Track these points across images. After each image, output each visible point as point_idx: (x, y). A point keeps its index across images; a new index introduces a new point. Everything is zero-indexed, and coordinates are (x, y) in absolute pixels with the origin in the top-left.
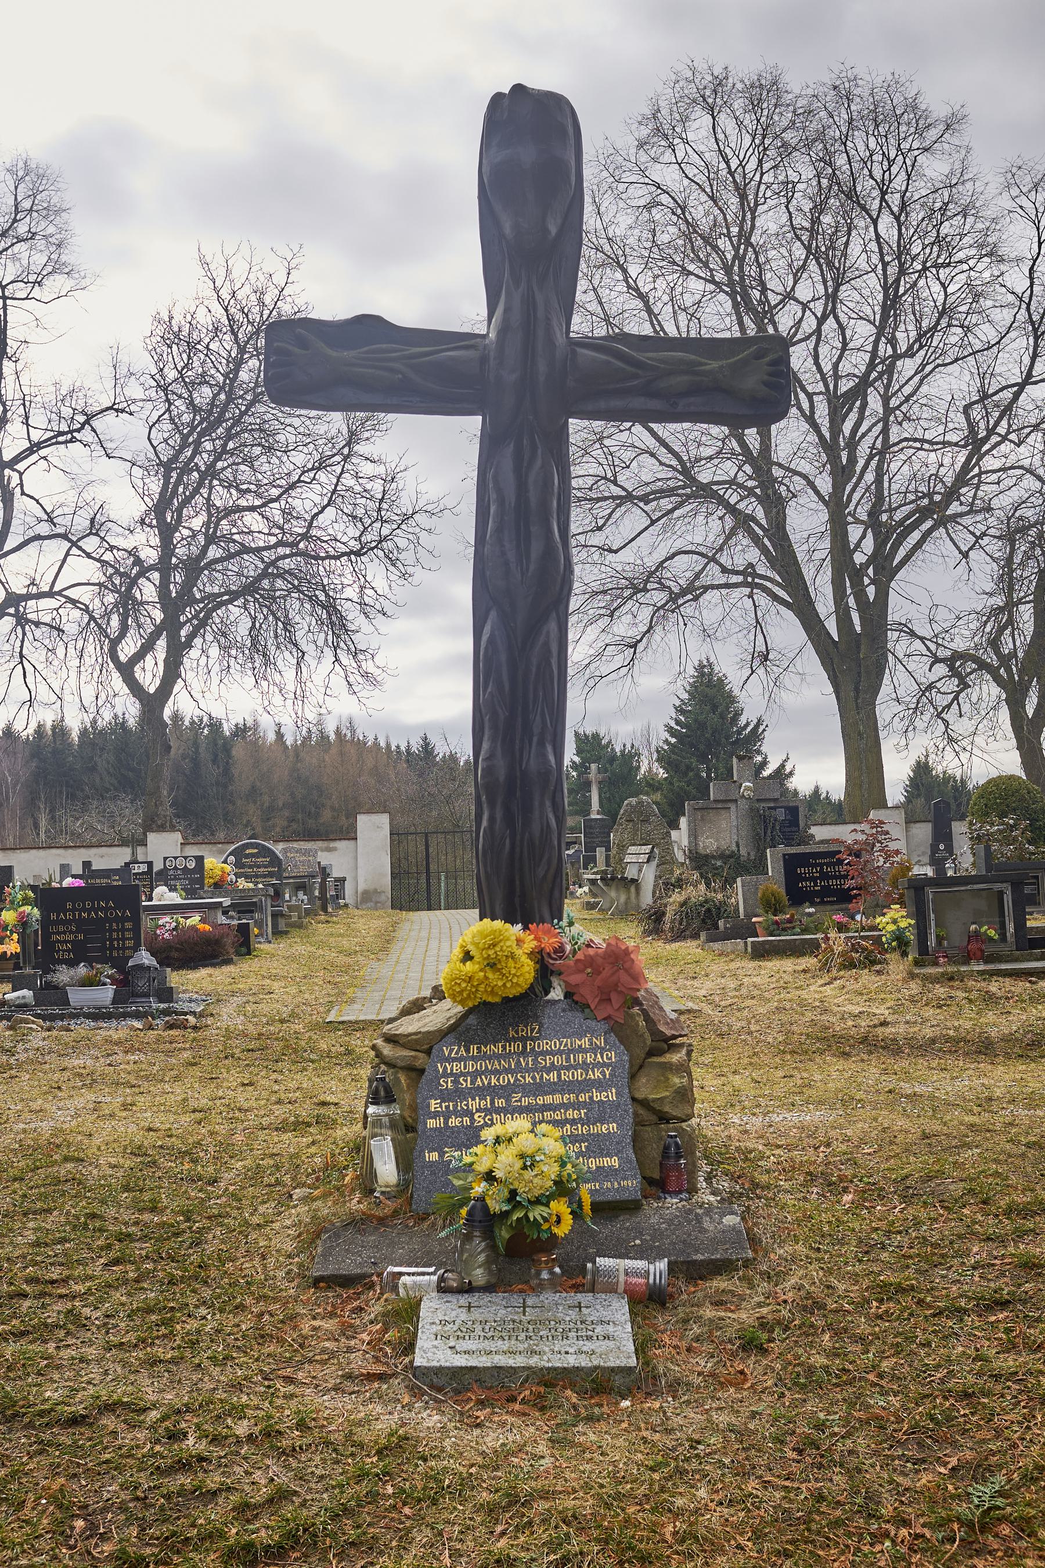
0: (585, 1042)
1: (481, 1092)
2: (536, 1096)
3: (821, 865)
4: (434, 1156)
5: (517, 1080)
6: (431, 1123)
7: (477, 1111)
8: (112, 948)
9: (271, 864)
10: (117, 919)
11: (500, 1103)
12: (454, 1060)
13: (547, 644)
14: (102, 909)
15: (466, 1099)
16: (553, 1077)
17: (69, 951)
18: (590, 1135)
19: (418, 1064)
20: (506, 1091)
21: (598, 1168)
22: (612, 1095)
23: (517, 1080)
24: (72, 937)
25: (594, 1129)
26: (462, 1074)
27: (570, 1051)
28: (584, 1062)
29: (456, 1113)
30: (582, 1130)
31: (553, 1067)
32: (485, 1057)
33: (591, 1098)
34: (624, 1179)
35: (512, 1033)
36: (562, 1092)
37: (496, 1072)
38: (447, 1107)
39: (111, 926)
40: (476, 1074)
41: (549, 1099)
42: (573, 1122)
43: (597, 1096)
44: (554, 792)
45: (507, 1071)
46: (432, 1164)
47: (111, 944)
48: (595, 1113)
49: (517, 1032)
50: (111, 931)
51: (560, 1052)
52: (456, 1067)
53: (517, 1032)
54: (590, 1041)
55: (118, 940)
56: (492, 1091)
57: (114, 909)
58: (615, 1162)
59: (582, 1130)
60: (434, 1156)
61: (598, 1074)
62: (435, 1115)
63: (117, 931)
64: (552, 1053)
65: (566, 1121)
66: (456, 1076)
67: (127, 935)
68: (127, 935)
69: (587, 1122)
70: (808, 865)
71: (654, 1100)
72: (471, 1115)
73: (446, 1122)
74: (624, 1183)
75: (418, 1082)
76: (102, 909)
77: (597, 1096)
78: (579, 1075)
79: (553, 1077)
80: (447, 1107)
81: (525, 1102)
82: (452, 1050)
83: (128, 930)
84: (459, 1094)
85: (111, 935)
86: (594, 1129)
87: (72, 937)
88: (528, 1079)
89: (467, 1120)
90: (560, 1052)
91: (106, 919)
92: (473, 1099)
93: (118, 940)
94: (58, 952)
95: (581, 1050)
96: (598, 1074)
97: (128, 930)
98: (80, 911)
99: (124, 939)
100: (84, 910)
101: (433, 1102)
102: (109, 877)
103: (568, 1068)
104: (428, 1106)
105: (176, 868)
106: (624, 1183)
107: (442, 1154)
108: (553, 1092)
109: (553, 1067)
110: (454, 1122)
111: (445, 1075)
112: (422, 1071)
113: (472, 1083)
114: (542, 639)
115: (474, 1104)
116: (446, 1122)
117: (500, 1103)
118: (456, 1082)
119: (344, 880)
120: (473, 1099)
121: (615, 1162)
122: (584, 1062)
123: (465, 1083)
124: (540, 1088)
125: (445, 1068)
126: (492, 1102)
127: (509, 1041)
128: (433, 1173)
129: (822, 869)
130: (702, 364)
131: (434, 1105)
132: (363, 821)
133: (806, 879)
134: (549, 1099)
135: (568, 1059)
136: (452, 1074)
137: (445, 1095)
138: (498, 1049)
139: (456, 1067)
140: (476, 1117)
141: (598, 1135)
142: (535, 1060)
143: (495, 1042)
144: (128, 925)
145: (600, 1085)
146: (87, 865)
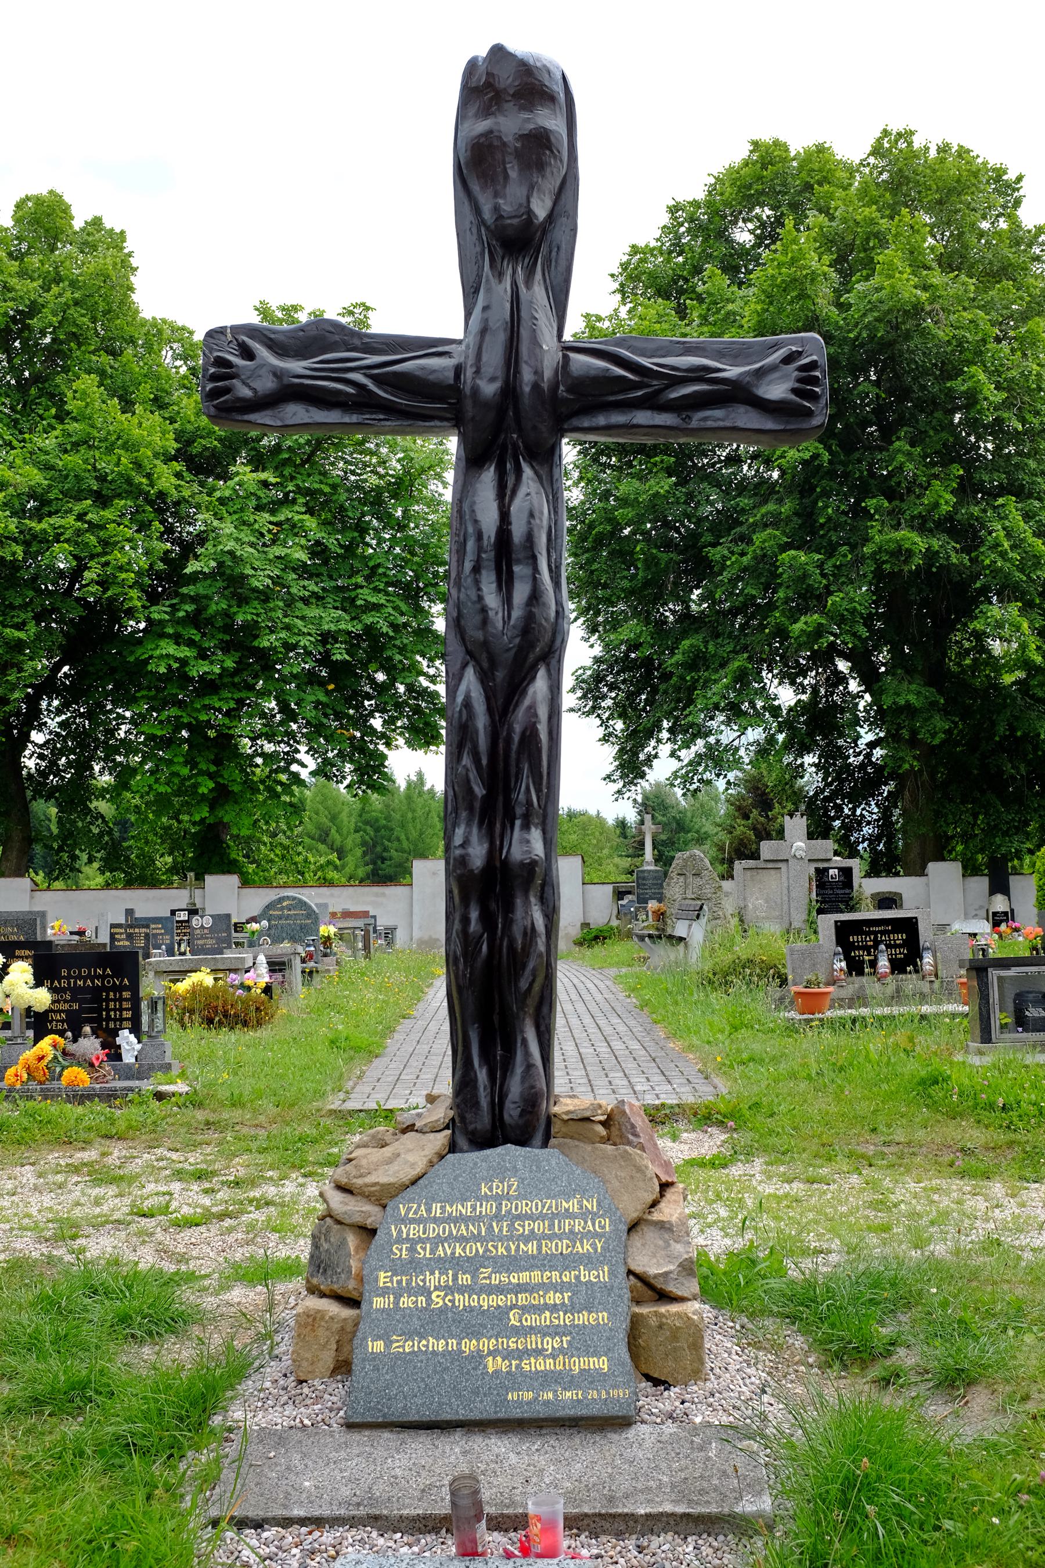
0: (573, 1205)
1: (442, 1264)
2: (509, 1271)
3: (875, 933)
4: (378, 1346)
5: (487, 1250)
6: (378, 1302)
7: (436, 1289)
8: (108, 1019)
9: (308, 916)
10: (115, 988)
11: (465, 1279)
12: (413, 1221)
13: (532, 710)
14: (98, 977)
15: (422, 1272)
16: (531, 1248)
17: (62, 1021)
18: (573, 1326)
19: (369, 1222)
20: (473, 1265)
21: (582, 1371)
22: (603, 1275)
23: (487, 1250)
24: (66, 1006)
25: (583, 1318)
26: (421, 1240)
27: (554, 1216)
28: (571, 1231)
29: (410, 1291)
30: (564, 1319)
31: (532, 1236)
32: (450, 1219)
33: (577, 1277)
34: (615, 1387)
35: (484, 1190)
36: (542, 1268)
37: (462, 1240)
38: (399, 1282)
39: (108, 995)
40: (438, 1241)
41: (524, 1277)
42: (553, 1309)
43: (585, 1276)
44: (543, 886)
45: (477, 1238)
46: (375, 1356)
47: (108, 1015)
48: (582, 1298)
49: (491, 1189)
50: (108, 1000)
51: (542, 1217)
52: (414, 1231)
53: (491, 1189)
54: (580, 1203)
55: (115, 1010)
56: (455, 1263)
57: (112, 977)
58: (602, 1364)
59: (564, 1319)
60: (378, 1346)
61: (587, 1247)
62: (384, 1292)
63: (115, 1000)
64: (531, 1217)
65: (546, 1307)
66: (413, 1243)
67: (126, 1005)
68: (125, 1005)
69: (571, 1308)
70: (861, 933)
71: (656, 1276)
72: (427, 1293)
73: (396, 1303)
74: (614, 1393)
75: (370, 1243)
76: (98, 977)
77: (585, 1276)
78: (563, 1246)
79: (531, 1248)
80: (399, 1282)
81: (495, 1280)
82: (409, 1209)
83: (126, 1000)
84: (414, 1265)
85: (107, 1005)
86: (583, 1318)
87: (66, 1006)
88: (501, 1250)
89: (422, 1300)
90: (542, 1217)
91: (103, 988)
92: (432, 1273)
93: (115, 1010)
94: (51, 1022)
95: (568, 1214)
96: (587, 1247)
97: (126, 1000)
98: (76, 978)
99: (121, 1010)
100: (80, 977)
101: (382, 1274)
102: (147, 927)
103: (550, 1238)
104: (377, 1280)
105: (202, 927)
106: (614, 1393)
107: (388, 1344)
108: (530, 1268)
109: (532, 1236)
110: (406, 1302)
111: (400, 1240)
112: (373, 1232)
113: (432, 1252)
114: (527, 702)
115: (432, 1280)
116: (396, 1303)
117: (465, 1279)
118: (412, 1250)
119: (394, 929)
120: (432, 1273)
121: (602, 1364)
122: (571, 1231)
123: (424, 1252)
124: (513, 1263)
125: (400, 1231)
126: (455, 1278)
127: (479, 1198)
128: (376, 1369)
129: (876, 937)
130: (724, 370)
131: (383, 1278)
132: (419, 867)
133: (859, 948)
134: (524, 1277)
135: (551, 1226)
136: (408, 1239)
137: (397, 1268)
138: (465, 1210)
139: (414, 1231)
140: (434, 1296)
141: (584, 1326)
142: (511, 1227)
143: (464, 1200)
144: (126, 994)
145: (589, 1261)
146: (129, 912)
